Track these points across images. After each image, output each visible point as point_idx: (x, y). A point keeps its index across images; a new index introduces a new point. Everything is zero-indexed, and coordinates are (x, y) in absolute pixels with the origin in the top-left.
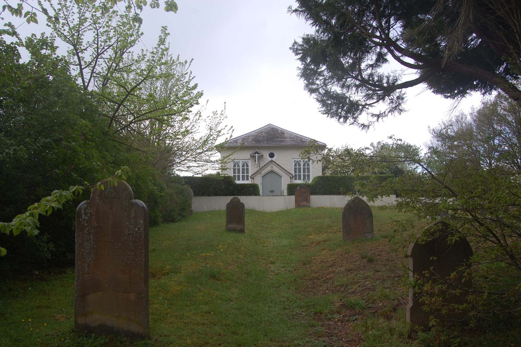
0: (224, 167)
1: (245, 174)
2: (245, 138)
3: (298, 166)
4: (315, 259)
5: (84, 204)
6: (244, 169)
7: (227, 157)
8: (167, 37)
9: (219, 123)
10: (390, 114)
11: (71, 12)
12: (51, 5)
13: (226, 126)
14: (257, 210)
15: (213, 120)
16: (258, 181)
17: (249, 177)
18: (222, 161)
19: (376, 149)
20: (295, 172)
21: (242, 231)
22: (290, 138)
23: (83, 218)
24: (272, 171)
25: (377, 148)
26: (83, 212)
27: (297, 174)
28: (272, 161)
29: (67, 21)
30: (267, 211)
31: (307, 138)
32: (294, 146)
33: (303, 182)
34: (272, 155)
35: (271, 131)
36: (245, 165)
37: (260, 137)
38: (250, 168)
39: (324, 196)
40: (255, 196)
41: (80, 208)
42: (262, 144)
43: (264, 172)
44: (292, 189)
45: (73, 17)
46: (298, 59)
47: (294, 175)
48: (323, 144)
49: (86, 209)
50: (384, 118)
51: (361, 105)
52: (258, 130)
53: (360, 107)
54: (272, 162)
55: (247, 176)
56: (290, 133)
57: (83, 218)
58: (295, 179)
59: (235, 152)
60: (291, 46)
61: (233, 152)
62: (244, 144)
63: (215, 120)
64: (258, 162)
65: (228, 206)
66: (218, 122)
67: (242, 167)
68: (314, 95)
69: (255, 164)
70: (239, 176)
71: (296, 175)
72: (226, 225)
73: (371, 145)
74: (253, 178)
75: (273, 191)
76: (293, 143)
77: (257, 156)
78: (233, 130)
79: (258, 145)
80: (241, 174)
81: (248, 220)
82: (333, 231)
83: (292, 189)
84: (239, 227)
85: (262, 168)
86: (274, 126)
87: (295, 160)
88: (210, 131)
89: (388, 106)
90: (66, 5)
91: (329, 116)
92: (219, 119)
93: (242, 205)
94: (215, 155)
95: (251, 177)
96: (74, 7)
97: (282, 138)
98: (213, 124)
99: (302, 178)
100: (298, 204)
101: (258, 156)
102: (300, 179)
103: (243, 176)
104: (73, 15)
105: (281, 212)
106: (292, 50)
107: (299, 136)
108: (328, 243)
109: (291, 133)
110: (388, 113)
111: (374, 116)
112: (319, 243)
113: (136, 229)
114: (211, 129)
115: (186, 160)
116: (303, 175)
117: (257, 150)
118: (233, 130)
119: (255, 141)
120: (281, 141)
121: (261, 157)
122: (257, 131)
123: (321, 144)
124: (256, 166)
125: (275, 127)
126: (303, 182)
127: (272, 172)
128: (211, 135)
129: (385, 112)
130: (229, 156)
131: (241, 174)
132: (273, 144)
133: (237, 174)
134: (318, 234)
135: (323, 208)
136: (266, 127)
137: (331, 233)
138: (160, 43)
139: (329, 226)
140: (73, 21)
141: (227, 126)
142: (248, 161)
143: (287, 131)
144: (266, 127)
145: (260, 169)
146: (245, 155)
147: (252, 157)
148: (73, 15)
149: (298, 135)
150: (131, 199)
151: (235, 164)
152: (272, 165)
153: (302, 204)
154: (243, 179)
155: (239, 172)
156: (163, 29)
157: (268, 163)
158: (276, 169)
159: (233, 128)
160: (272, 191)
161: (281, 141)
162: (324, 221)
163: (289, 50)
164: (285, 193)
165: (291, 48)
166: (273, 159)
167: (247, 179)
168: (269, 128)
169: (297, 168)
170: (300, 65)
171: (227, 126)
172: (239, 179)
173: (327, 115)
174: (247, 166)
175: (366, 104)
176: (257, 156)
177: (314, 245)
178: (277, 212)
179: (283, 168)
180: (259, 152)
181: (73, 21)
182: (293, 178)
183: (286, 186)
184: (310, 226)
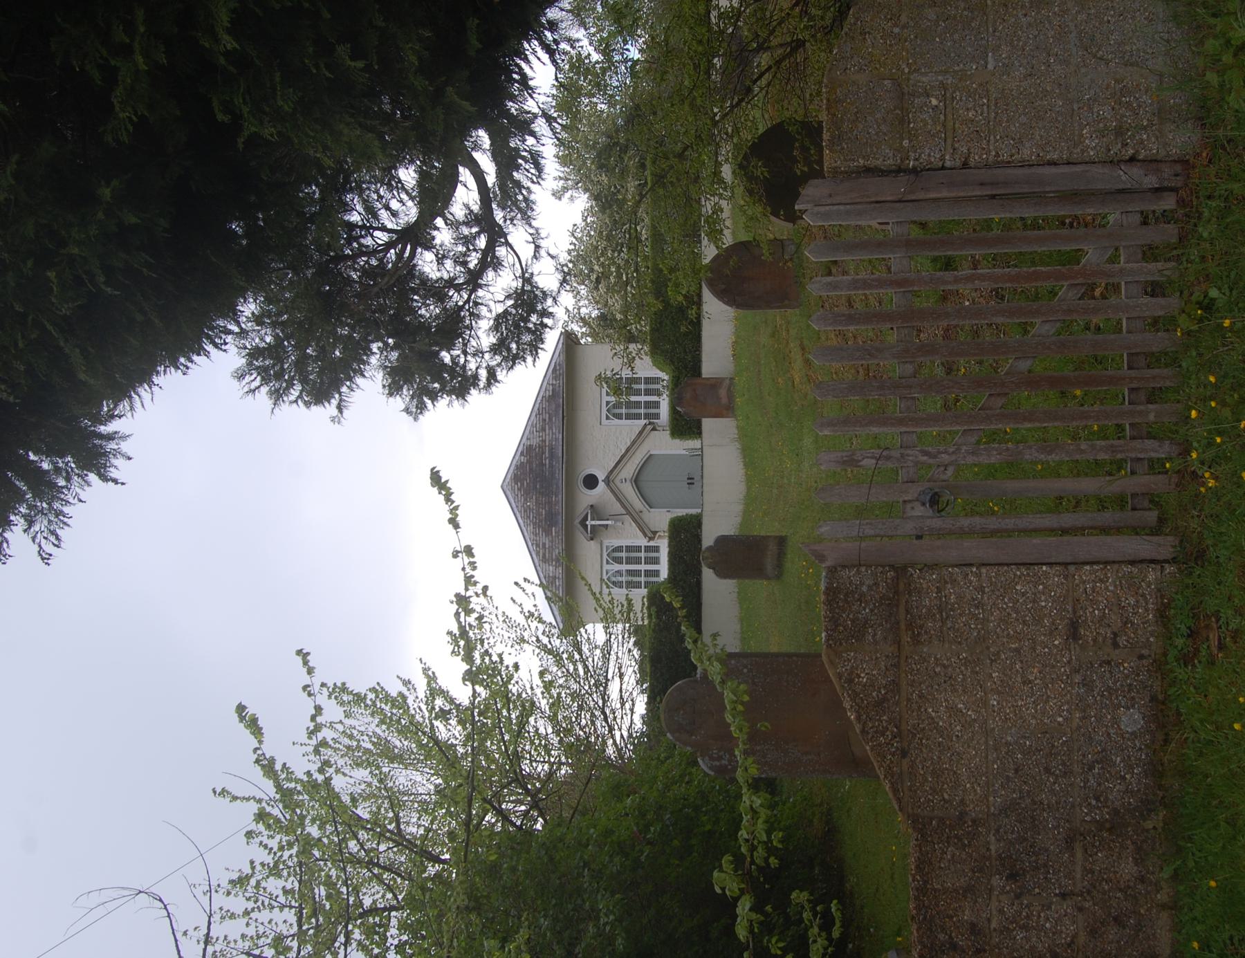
0: (623, 606)
1: (643, 555)
2: (541, 555)
3: (622, 408)
4: (836, 373)
5: (703, 760)
6: (627, 558)
7: (597, 600)
8: (350, 690)
9: (506, 619)
10: (534, 223)
11: (270, 927)
13: (514, 601)
14: (739, 520)
16: (661, 519)
17: (652, 543)
19: (569, 181)
20: (638, 417)
21: (782, 541)
22: (543, 429)
23: (727, 763)
24: (635, 481)
25: (567, 179)
26: (718, 763)
27: (642, 411)
28: (607, 481)
30: (744, 493)
32: (567, 420)
33: (665, 395)
34: (591, 482)
36: (615, 555)
37: (539, 514)
38: (624, 543)
41: (710, 768)
42: (560, 508)
43: (637, 503)
45: (280, 923)
46: (434, 405)
47: (646, 421)
48: (561, 341)
49: (712, 758)
50: (542, 235)
52: (519, 519)
54: (609, 481)
55: (648, 549)
56: (527, 432)
57: (727, 763)
58: (658, 419)
59: (583, 578)
60: (411, 418)
62: (557, 560)
63: (497, 631)
64: (608, 520)
65: (722, 573)
66: (504, 621)
67: (621, 563)
68: (500, 375)
70: (648, 573)
71: (645, 414)
72: (768, 578)
74: (655, 533)
75: (688, 479)
76: (557, 421)
77: (593, 523)
79: (561, 519)
80: (643, 567)
81: (759, 530)
82: (784, 327)
83: (685, 426)
84: (773, 547)
86: (509, 476)
87: (604, 417)
88: (528, 642)
89: (521, 228)
90: (252, 938)
91: (541, 346)
93: (722, 540)
94: (592, 633)
95: (651, 539)
96: (257, 919)
97: (543, 453)
98: (506, 635)
99: (654, 398)
100: (725, 410)
101: (593, 519)
102: (656, 405)
103: (650, 561)
104: (276, 923)
105: (744, 457)
106: (420, 416)
107: (537, 406)
108: (806, 342)
109: (528, 428)
110: (533, 227)
111: (537, 255)
112: (807, 362)
113: (745, 670)
116: (645, 395)
117: (577, 521)
118: (525, 580)
119: (551, 526)
120: (552, 456)
121: (595, 511)
123: (560, 345)
124: (619, 524)
125: (511, 471)
126: (665, 395)
127: (637, 481)
128: (538, 640)
129: (531, 234)
131: (643, 567)
132: (560, 476)
133: (643, 579)
134: (790, 363)
136: (510, 496)
137: (788, 331)
138: (362, 705)
139: (773, 335)
140: (288, 924)
141: (512, 599)
144: (510, 496)
145: (629, 513)
146: (590, 555)
147: (594, 534)
148: (276, 923)
149: (536, 409)
150: (696, 681)
152: (617, 481)
153: (724, 400)
154: (656, 561)
155: (636, 573)
156: (333, 697)
157: (612, 491)
158: (629, 470)
159: (521, 582)
160: (691, 481)
161: (552, 456)
162: (764, 345)
163: (419, 421)
164: (695, 444)
165: (416, 419)
166: (601, 476)
167: (656, 549)
168: (513, 489)
169: (627, 411)
171: (512, 599)
172: (656, 573)
173: (539, 351)
174: (619, 549)
175: (523, 276)
176: (593, 523)
177: (810, 373)
178: (744, 465)
179: (628, 450)
181: (288, 924)
182: (653, 423)
183: (677, 441)
184: (773, 380)
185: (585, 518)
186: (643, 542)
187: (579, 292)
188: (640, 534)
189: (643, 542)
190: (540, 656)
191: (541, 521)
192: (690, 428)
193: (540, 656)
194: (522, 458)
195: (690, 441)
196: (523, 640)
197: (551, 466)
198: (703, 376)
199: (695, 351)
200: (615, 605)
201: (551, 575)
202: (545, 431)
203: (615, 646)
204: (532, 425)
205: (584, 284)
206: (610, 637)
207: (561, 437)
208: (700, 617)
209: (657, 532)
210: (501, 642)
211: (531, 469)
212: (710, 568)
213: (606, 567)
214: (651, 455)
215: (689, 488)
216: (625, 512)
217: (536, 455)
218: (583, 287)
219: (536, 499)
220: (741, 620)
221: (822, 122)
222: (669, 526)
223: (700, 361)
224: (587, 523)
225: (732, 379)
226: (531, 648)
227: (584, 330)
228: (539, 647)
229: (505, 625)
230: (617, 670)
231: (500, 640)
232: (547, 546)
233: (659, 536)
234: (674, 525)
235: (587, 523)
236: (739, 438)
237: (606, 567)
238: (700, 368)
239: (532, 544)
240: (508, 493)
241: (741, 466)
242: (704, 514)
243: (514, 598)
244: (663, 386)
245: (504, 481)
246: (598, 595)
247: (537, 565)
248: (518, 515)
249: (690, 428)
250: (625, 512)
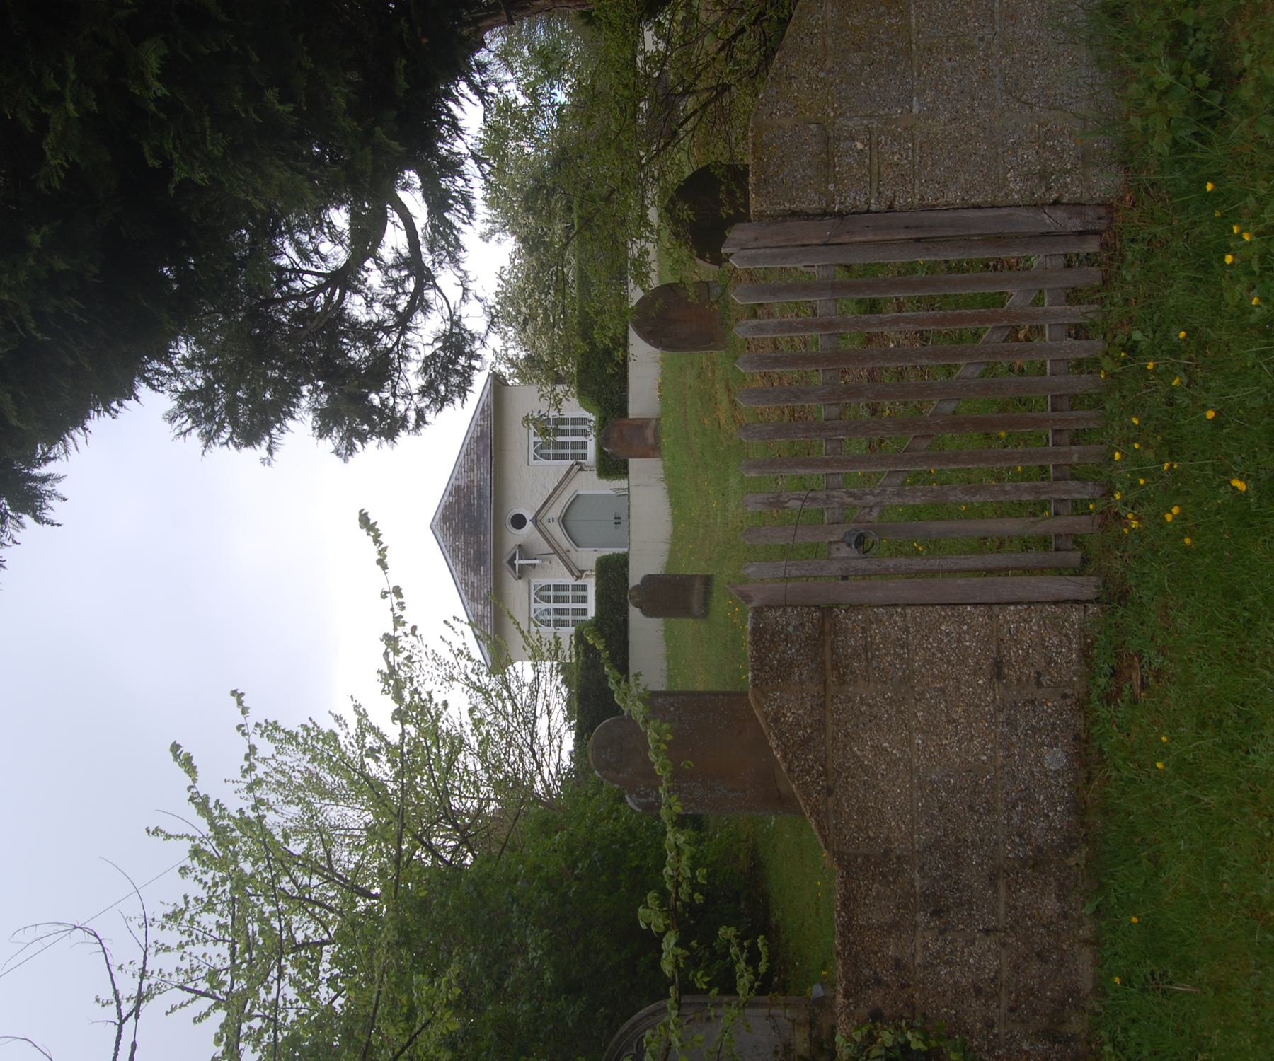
0: (551, 644)
1: (570, 593)
2: (470, 594)
7: (526, 638)
9: (435, 657)
10: (462, 266)
12: (181, 1005)
13: (443, 640)
14: (665, 559)
15: (426, 673)
16: (588, 558)
17: (579, 582)
18: (536, 657)
20: (565, 457)
22: (472, 470)
24: (563, 521)
25: (495, 222)
28: (535, 521)
29: (221, 971)
31: (473, 424)
33: (592, 436)
34: (519, 521)
35: (451, 524)
36: (543, 594)
39: (630, 381)
40: (630, 566)
41: (638, 805)
42: (488, 547)
43: (565, 543)
44: (612, 466)
45: (214, 957)
47: (573, 462)
49: (639, 795)
50: (470, 278)
51: (451, 328)
53: (456, 330)
55: (575, 588)
56: (456, 472)
58: (585, 459)
59: (511, 617)
60: (341, 460)
61: (512, 621)
62: (486, 599)
63: (426, 669)
65: (649, 612)
66: (434, 659)
68: (429, 416)
69: (542, 566)
70: (575, 612)
72: (695, 617)
73: (487, 241)
74: (582, 572)
76: (485, 461)
77: (521, 562)
78: (454, 618)
79: (489, 558)
80: (570, 606)
83: (612, 466)
84: (698, 586)
85: (552, 547)
86: (438, 516)
87: (531, 457)
92: (424, 656)
93: (648, 579)
94: (520, 671)
95: (578, 578)
97: (472, 493)
100: (651, 451)
101: (521, 558)
105: (670, 498)
112: (733, 403)
113: (672, 709)
114: (452, 678)
115: (531, 746)
117: (505, 561)
118: (454, 618)
119: (479, 565)
120: (480, 496)
121: (523, 550)
122: (449, 560)
123: (488, 387)
124: (547, 563)
126: (592, 436)
127: (564, 521)
128: (467, 678)
130: (522, 632)
131: (570, 606)
132: (488, 515)
133: (570, 618)
135: (661, 385)
136: (439, 536)
137: (714, 372)
139: (699, 376)
142: (532, 588)
143: (453, 479)
144: (439, 536)
145: (556, 552)
146: (518, 594)
147: (522, 573)
149: (464, 449)
151: (542, 622)
152: (545, 521)
153: (651, 441)
154: (583, 600)
155: (565, 612)
157: (540, 531)
158: (556, 510)
160: (618, 521)
161: (480, 496)
164: (621, 484)
165: (345, 461)
166: (529, 516)
167: (584, 588)
170: (373, 443)
172: (584, 612)
174: (547, 588)
176: (521, 562)
179: (555, 490)
180: (510, 556)
182: (580, 464)
185: (513, 558)
186: (570, 581)
188: (568, 573)
189: (570, 581)
191: (469, 560)
209: (584, 571)
213: (534, 606)
218: (510, 328)
222: (597, 565)
223: (627, 402)
225: (658, 420)
230: (545, 708)
237: (534, 606)
240: (437, 533)
241: (668, 506)
248: (447, 554)
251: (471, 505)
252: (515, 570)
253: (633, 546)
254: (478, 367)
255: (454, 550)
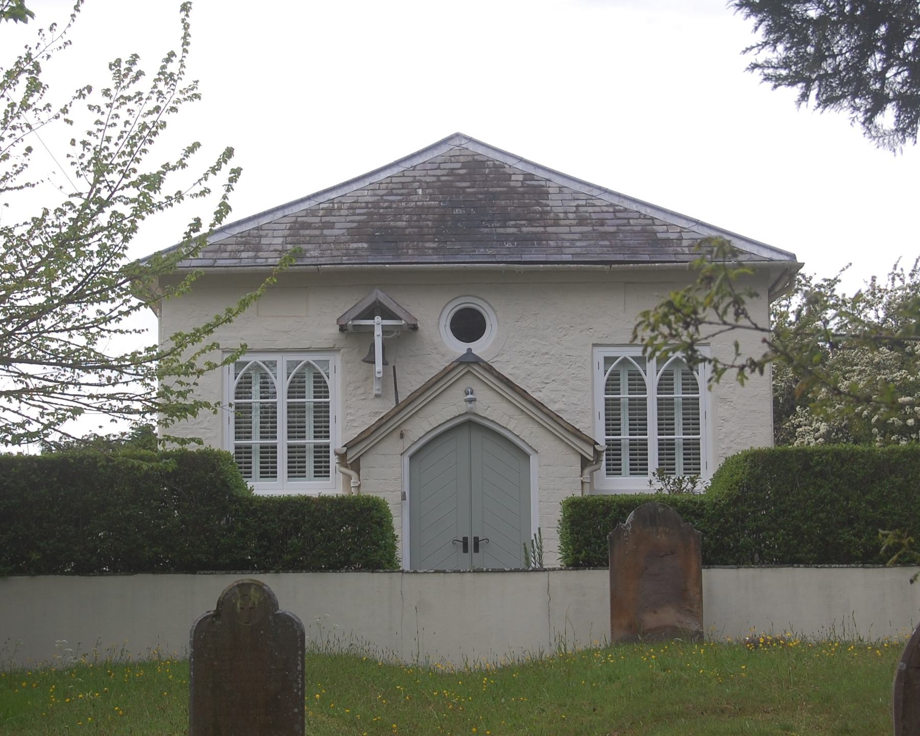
0: (181, 394)
1: (310, 441)
7: (196, 337)
17: (333, 460)
20: (612, 425)
22: (581, 221)
27: (625, 436)
28: (469, 361)
31: (683, 223)
33: (659, 485)
35: (462, 178)
52: (388, 173)
54: (468, 363)
55: (322, 452)
59: (244, 305)
62: (299, 254)
63: (123, 112)
64: (385, 363)
66: (144, 126)
70: (269, 453)
74: (356, 466)
75: (476, 539)
76: (600, 250)
77: (378, 331)
79: (385, 261)
80: (282, 441)
86: (480, 150)
92: (151, 105)
95: (342, 457)
97: (531, 222)
98: (114, 133)
101: (386, 331)
102: (638, 467)
105: (523, 668)
107: (634, 207)
109: (585, 190)
116: (661, 443)
117: (379, 295)
118: (237, 172)
120: (525, 240)
122: (383, 176)
123: (766, 254)
124: (376, 388)
126: (659, 485)
128: (103, 204)
130: (209, 330)
131: (282, 441)
133: (256, 441)
135: (779, 645)
136: (436, 153)
141: (197, 145)
144: (436, 153)
145: (400, 408)
152: (468, 382)
153: (650, 620)
154: (296, 470)
155: (269, 430)
157: (446, 372)
159: (233, 163)
160: (472, 545)
161: (525, 240)
164: (553, 555)
166: (479, 348)
167: (322, 471)
168: (451, 158)
171: (197, 145)
172: (269, 472)
174: (321, 388)
176: (378, 331)
179: (538, 405)
180: (393, 307)
182: (598, 460)
185: (387, 314)
186: (337, 441)
187: (871, 306)
188: (354, 434)
189: (337, 441)
190: (66, 208)
191: (382, 217)
192: (588, 543)
193: (66, 208)
194: (521, 178)
195: (559, 543)
196: (100, 167)
197: (506, 237)
198: (704, 572)
199: (760, 553)
200: (183, 378)
201: (264, 241)
202: (579, 224)
203: (92, 378)
204: (592, 197)
205: (887, 316)
206: (112, 368)
207: (568, 258)
208: (164, 570)
209: (358, 471)
210: (98, 122)
211: (495, 196)
212: (220, 603)
213: (282, 361)
214: (527, 456)
215: (454, 542)
216: (401, 399)
217: (527, 206)
218: (881, 314)
219: (429, 207)
220: (149, 666)
221: (97, 257)
222: (368, 499)
223: (739, 563)
224: (378, 319)
225: (699, 636)
226: (85, 188)
227: (792, 318)
228: (85, 206)
229: (136, 128)
230: (40, 384)
231: (103, 119)
232: (326, 232)
233: (350, 477)
234: (370, 509)
235: (378, 319)
236: (565, 656)
237: (282, 361)
238: (723, 563)
239: (331, 201)
240: (444, 149)
241: (502, 660)
242: (396, 576)
243: (198, 151)
244: (680, 482)
245: (470, 140)
246: (206, 341)
247: (287, 212)
248: (395, 171)
249: (588, 543)
250: (401, 399)
251: (505, 219)
252: (359, 317)
253: (410, 581)
254: (879, 119)
255: (404, 185)
